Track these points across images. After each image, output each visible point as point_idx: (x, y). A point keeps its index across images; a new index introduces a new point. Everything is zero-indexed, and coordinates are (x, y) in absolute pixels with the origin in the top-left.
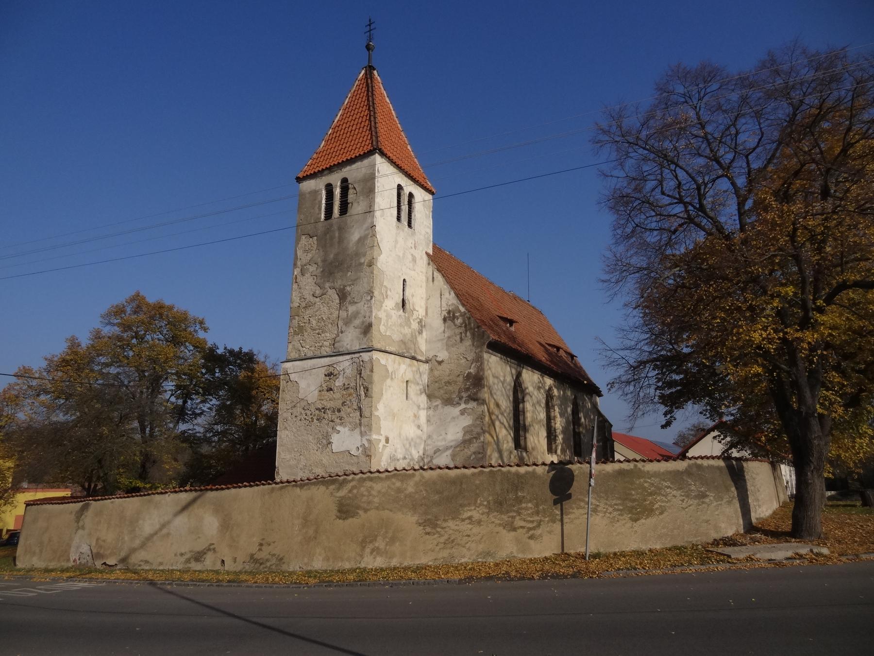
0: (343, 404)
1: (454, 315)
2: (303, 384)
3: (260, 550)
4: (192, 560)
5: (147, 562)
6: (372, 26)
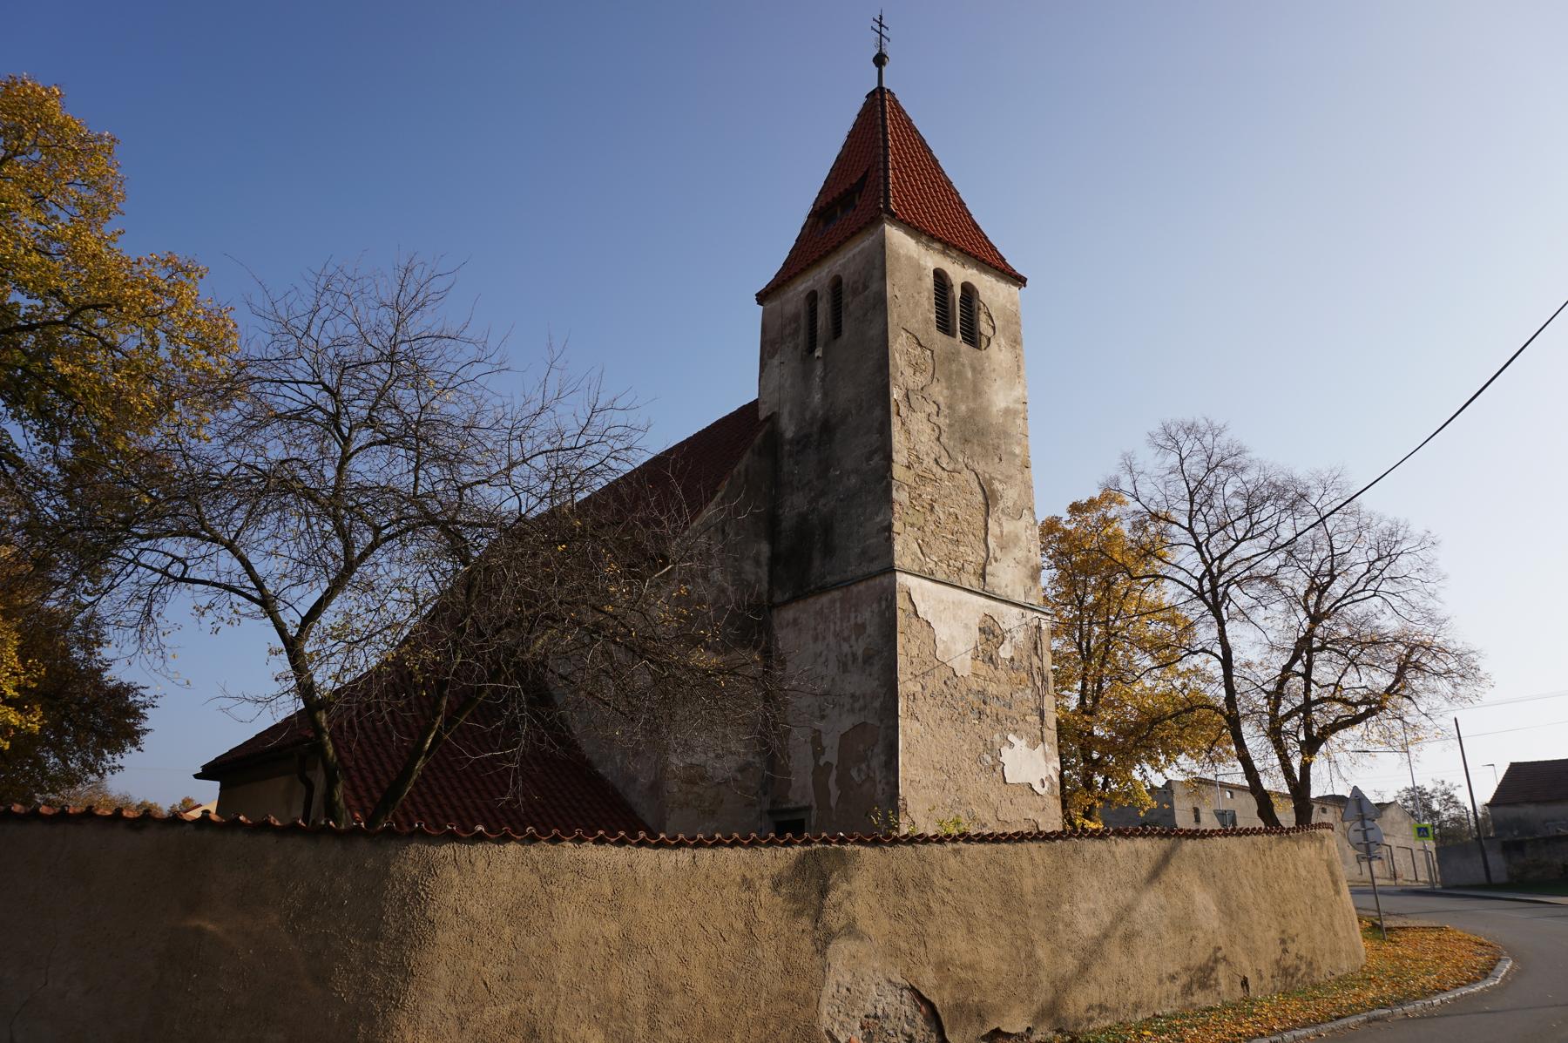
2: (942, 632)
3: (1285, 951)
4: (1195, 987)
5: (1102, 1008)
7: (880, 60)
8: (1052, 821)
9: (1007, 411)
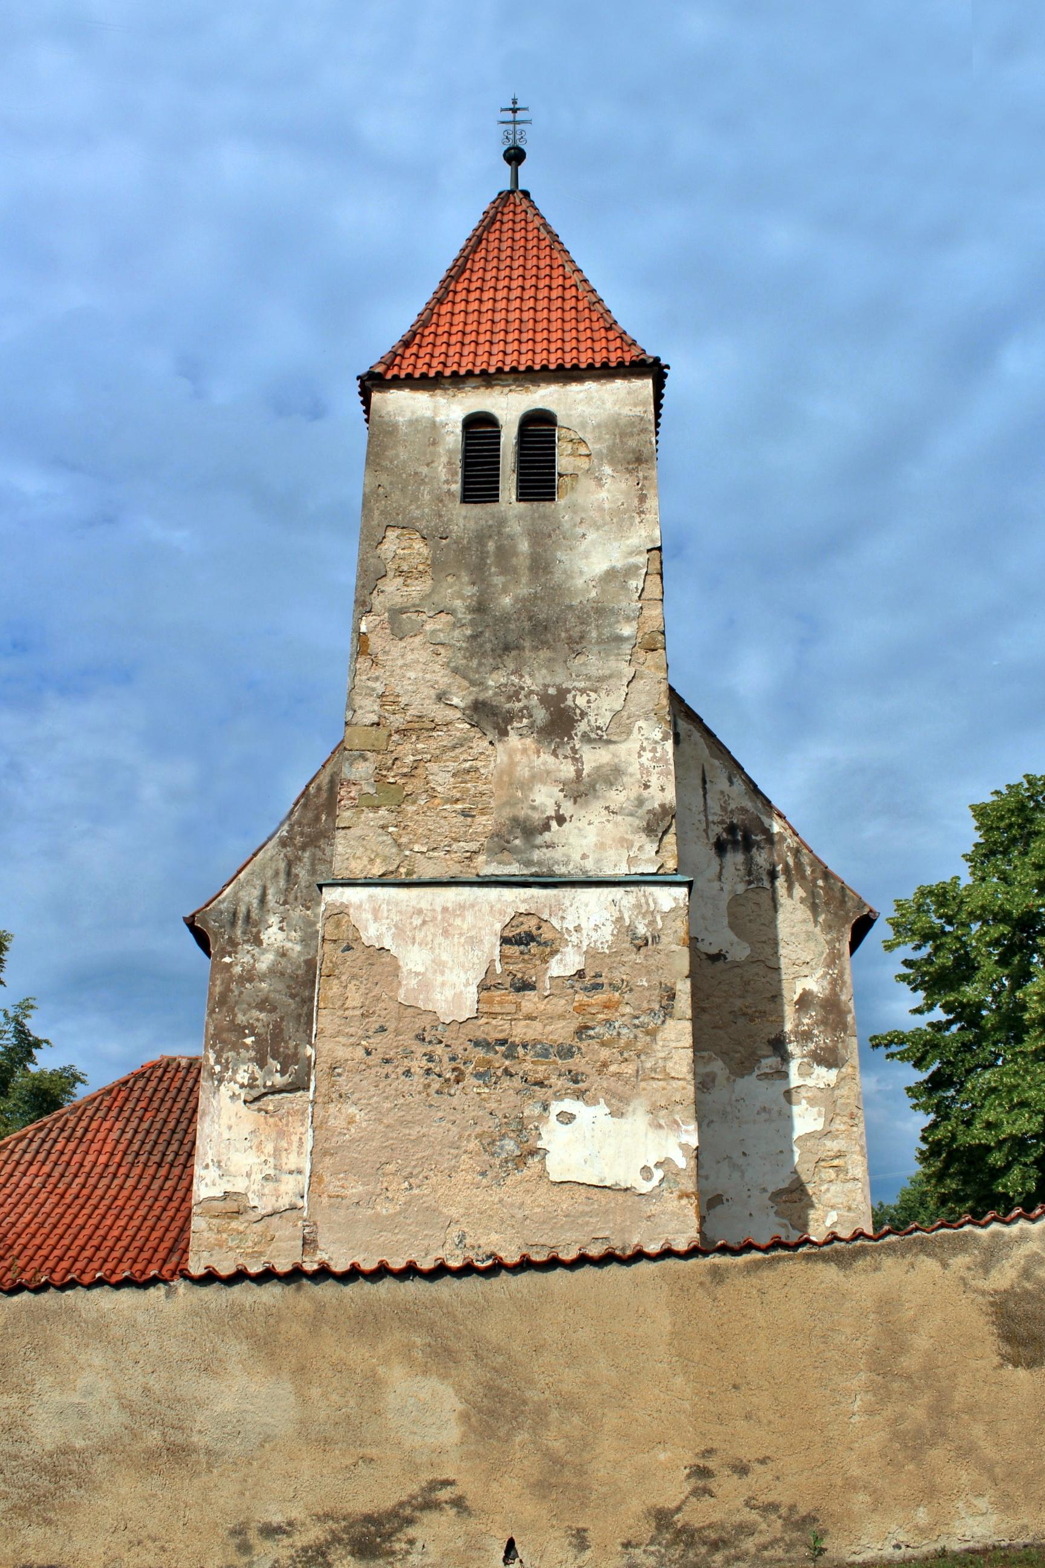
0: (581, 1031)
1: (746, 837)
2: (413, 960)
6: (520, 116)
9: (611, 574)
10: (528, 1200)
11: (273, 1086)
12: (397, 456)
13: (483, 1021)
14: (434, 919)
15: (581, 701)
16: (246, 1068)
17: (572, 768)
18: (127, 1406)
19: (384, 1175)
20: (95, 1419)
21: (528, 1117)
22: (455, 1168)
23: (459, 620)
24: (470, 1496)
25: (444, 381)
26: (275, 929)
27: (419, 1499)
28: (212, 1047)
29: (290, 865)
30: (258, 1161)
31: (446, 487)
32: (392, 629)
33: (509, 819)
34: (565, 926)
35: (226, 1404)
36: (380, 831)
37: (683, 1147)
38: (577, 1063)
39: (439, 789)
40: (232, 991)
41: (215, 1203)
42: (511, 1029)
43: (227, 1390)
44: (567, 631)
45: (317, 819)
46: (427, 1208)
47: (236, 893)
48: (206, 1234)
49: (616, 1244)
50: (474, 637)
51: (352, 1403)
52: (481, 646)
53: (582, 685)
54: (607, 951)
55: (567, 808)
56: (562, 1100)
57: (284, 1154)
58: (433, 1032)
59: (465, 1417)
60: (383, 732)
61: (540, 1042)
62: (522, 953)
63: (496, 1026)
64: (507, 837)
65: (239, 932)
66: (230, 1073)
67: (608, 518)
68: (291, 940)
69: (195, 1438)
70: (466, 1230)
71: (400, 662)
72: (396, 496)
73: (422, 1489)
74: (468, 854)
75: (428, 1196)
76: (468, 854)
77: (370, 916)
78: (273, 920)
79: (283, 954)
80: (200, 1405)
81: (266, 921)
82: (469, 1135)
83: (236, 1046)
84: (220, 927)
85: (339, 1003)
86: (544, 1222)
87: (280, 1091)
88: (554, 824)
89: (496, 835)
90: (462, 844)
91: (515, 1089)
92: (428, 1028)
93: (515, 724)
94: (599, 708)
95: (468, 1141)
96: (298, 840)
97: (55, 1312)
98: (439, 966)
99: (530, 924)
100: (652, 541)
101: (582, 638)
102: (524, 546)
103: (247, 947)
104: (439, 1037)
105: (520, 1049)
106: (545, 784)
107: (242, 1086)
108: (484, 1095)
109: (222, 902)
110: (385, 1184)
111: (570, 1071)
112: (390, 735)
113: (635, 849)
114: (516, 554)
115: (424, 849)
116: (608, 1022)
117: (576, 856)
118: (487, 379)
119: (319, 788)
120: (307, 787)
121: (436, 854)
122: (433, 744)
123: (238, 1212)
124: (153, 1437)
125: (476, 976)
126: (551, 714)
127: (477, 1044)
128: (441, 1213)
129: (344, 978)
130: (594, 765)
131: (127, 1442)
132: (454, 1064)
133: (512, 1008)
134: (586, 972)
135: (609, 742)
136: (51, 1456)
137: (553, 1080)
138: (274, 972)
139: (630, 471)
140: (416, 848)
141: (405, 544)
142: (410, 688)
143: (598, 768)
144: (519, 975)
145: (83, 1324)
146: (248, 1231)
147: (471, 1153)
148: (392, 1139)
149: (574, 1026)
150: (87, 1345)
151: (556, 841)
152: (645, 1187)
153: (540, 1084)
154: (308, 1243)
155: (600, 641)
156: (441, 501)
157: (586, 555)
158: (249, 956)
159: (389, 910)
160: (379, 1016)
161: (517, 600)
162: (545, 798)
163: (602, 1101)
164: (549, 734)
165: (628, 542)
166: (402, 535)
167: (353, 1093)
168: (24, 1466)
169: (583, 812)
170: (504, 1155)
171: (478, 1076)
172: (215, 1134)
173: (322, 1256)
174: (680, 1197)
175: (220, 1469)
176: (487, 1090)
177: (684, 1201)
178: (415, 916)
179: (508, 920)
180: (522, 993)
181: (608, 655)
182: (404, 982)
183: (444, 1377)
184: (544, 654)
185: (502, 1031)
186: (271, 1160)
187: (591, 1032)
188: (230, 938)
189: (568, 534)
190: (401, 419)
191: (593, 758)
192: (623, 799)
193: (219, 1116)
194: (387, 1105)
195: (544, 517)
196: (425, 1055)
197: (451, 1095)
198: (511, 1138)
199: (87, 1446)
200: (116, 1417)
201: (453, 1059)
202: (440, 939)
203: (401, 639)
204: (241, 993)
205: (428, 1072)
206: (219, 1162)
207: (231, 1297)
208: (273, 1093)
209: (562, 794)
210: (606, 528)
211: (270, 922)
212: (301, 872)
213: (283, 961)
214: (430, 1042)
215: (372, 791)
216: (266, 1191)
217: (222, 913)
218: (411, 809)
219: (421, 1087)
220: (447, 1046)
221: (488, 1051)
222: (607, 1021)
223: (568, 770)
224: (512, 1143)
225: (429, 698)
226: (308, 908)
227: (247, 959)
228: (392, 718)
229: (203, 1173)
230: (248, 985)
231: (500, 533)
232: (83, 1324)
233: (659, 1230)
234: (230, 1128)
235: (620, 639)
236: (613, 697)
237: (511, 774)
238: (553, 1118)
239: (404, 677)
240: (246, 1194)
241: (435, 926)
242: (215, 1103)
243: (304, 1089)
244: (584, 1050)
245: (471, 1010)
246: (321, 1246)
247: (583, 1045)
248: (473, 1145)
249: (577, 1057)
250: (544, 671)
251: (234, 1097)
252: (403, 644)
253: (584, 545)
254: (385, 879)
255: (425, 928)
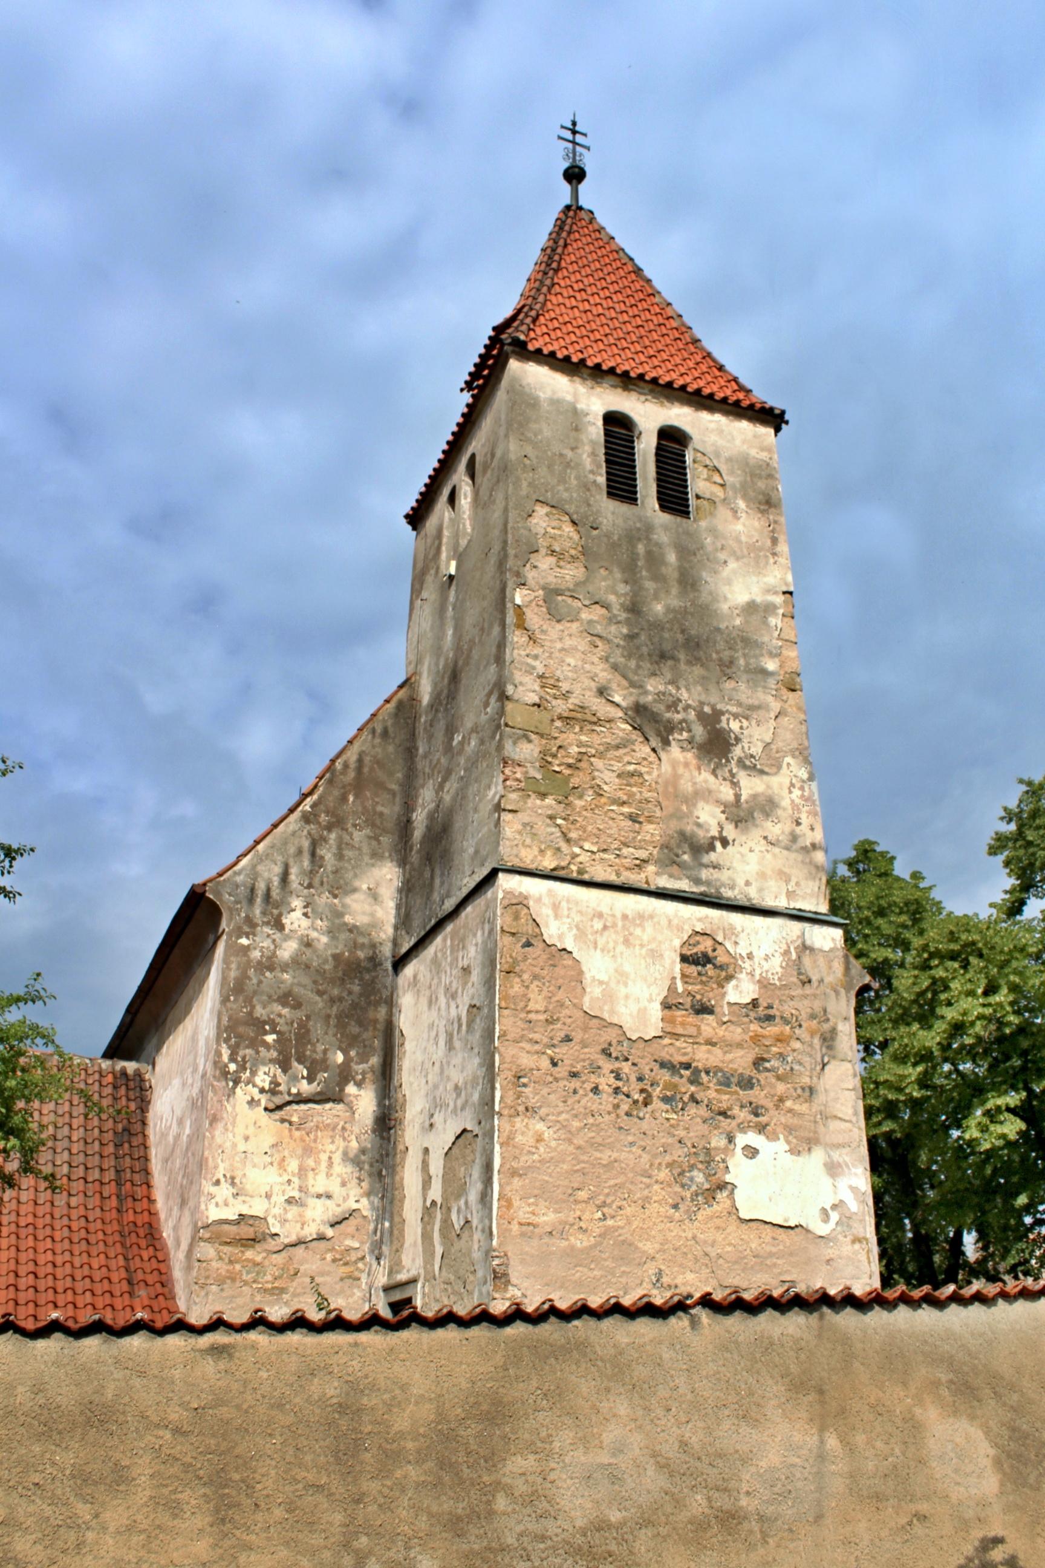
0: (758, 1062)
2: (596, 966)
6: (579, 138)
7: (575, 175)
8: (865, 1277)
9: (751, 608)
10: (719, 1237)
11: (299, 1094)
12: (541, 431)
13: (667, 1041)
14: (614, 925)
15: (735, 725)
16: (267, 1070)
17: (731, 792)
18: (664, 1466)
19: (576, 1202)
20: (630, 1483)
21: (715, 1148)
22: (647, 1199)
23: (615, 616)
24: (1021, 1556)
25: (584, 370)
26: (298, 914)
27: (976, 1562)
28: (227, 1041)
29: (314, 845)
30: (280, 1180)
31: (591, 476)
32: (548, 609)
33: (677, 832)
34: (738, 951)
35: (771, 1458)
36: (548, 821)
37: (854, 1189)
38: (757, 1095)
39: (605, 787)
40: (250, 979)
41: (226, 1227)
42: (694, 1053)
43: (769, 1440)
44: (718, 652)
45: (344, 799)
46: (623, 1242)
47: (254, 867)
48: (215, 1264)
49: (801, 1289)
50: (631, 637)
51: (897, 1451)
52: (638, 648)
53: (734, 709)
54: (778, 983)
55: (730, 831)
56: (745, 1133)
57: (311, 1174)
58: (619, 1048)
59: (998, 1463)
60: (546, 716)
61: (721, 1070)
62: (699, 974)
63: (679, 1049)
64: (676, 850)
65: (257, 912)
66: (248, 1073)
67: (745, 551)
68: (316, 930)
69: (744, 1502)
70: (663, 1267)
71: (559, 645)
72: (543, 471)
73: (976, 1549)
74: (638, 862)
75: (622, 1228)
76: (638, 862)
77: (550, 912)
78: (297, 903)
79: (308, 944)
80: (745, 1461)
81: (289, 904)
82: (660, 1164)
83: (256, 1043)
84: (237, 902)
85: (522, 1004)
86: (736, 1262)
87: (307, 1101)
88: (718, 845)
89: (665, 846)
90: (631, 850)
91: (701, 1117)
92: (614, 1042)
93: (676, 736)
94: (752, 737)
95: (659, 1170)
96: (323, 818)
97: (562, 1346)
98: (622, 976)
99: (706, 945)
100: (787, 584)
101: (731, 662)
102: (672, 557)
103: (267, 930)
104: (626, 1054)
105: (703, 1074)
106: (707, 802)
107: (262, 1091)
108: (672, 1122)
109: (239, 873)
110: (578, 1213)
111: (751, 1103)
112: (553, 720)
113: (793, 883)
114: (663, 562)
115: (595, 849)
116: (782, 1056)
117: (741, 882)
118: (627, 381)
119: (346, 766)
120: (333, 761)
121: (606, 856)
122: (596, 740)
123: (254, 1240)
124: (698, 1503)
125: (660, 993)
126: (709, 733)
127: (663, 1065)
128: (637, 1248)
129: (525, 976)
130: (751, 792)
131: (669, 1510)
132: (641, 1085)
133: (692, 1031)
134: (760, 1001)
135: (762, 772)
136: (585, 1535)
137: (736, 1111)
138: (296, 963)
139: (762, 512)
140: (587, 846)
141: (555, 523)
142: (570, 674)
143: (755, 796)
144: (698, 997)
145: (599, 1363)
146: (267, 1263)
147: (662, 1183)
148: (583, 1162)
149: (751, 1057)
150: (608, 1390)
151: (721, 863)
152: (822, 1229)
153: (723, 1114)
154: (500, 1278)
155: (748, 670)
156: (589, 490)
157: (729, 582)
158: (269, 941)
159: (569, 909)
160: (564, 1024)
161: (668, 610)
162: (709, 817)
163: (781, 1136)
164: (709, 753)
165: (766, 579)
166: (551, 513)
167: (540, 1107)
168: (554, 1549)
169: (744, 838)
170: (694, 1188)
171: (666, 1100)
172: (228, 1144)
173: (513, 1292)
174: (853, 1242)
175: (776, 1539)
176: (675, 1117)
177: (857, 1246)
178: (596, 920)
179: (686, 938)
180: (701, 1016)
181: (756, 686)
182: (588, 990)
183: (972, 1418)
184: (698, 670)
185: (685, 1054)
186: (295, 1180)
187: (767, 1065)
188: (247, 917)
189: (711, 557)
190: (542, 395)
191: (750, 786)
192: (779, 832)
193: (234, 1124)
194: (576, 1124)
195: (687, 533)
196: (612, 1072)
197: (640, 1119)
198: (699, 1170)
199: (624, 1517)
200: (653, 1480)
201: (640, 1079)
202: (621, 948)
203: (559, 621)
204: (260, 982)
205: (617, 1090)
206: (233, 1178)
207: (758, 1329)
208: (298, 1102)
209: (723, 816)
210: (745, 560)
211: (293, 905)
212: (327, 854)
213: (308, 952)
214: (617, 1058)
215: (539, 776)
216: (289, 1216)
217: (237, 886)
218: (579, 803)
219: (610, 1108)
220: (634, 1064)
221: (673, 1074)
222: (781, 1054)
223: (727, 793)
224: (701, 1175)
225: (590, 690)
226: (335, 896)
227: (267, 943)
228: (554, 702)
229: (213, 1189)
230: (268, 974)
231: (648, 539)
232: (599, 1363)
233: (838, 1275)
234: (247, 1138)
235: (764, 672)
236: (762, 728)
237: (675, 787)
238: (738, 1150)
239: (563, 661)
240: (265, 1219)
241: (616, 932)
242: (229, 1108)
243: (334, 1101)
244: (763, 1082)
245: (656, 1028)
246: (514, 1280)
247: (761, 1077)
248: (664, 1174)
249: (757, 1088)
250: (699, 688)
251: (252, 1102)
252: (559, 627)
253: (726, 572)
254: (555, 873)
255: (606, 933)
